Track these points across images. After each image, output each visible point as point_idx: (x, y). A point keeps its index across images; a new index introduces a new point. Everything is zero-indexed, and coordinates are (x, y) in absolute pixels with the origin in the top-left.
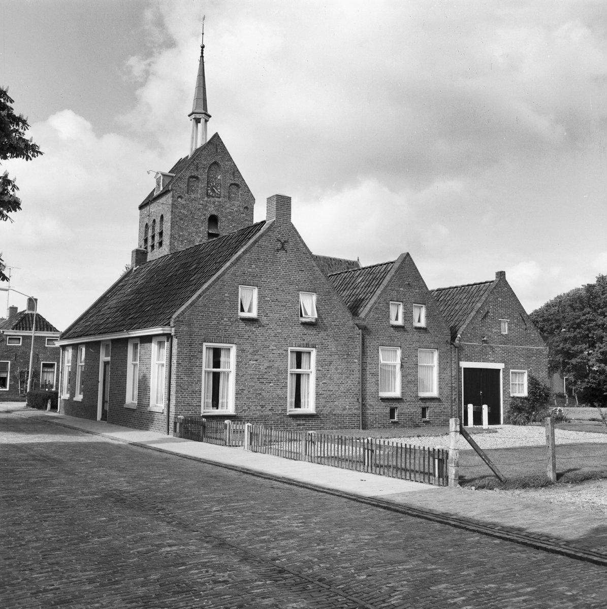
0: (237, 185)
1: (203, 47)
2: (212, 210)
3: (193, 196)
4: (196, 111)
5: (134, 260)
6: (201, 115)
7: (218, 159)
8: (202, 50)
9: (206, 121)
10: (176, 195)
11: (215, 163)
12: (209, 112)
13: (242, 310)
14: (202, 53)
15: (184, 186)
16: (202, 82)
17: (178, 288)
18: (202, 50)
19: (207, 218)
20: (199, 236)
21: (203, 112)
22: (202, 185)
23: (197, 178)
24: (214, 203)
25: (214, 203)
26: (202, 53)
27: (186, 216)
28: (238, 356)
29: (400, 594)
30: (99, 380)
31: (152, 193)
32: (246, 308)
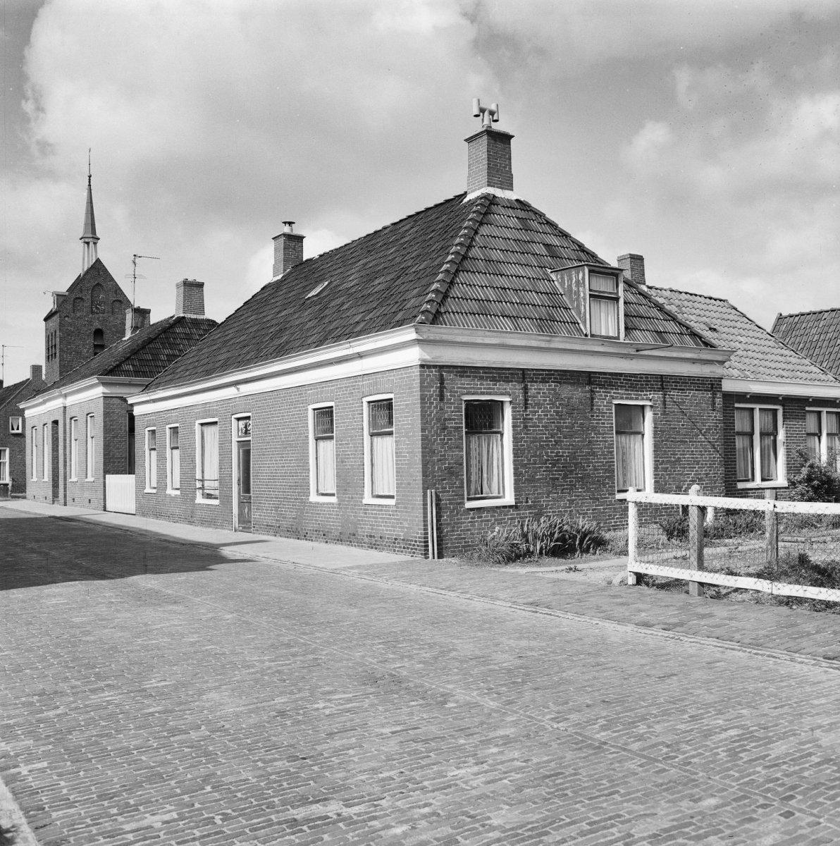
0: (120, 301)
1: (90, 177)
2: (97, 325)
3: (78, 314)
4: (86, 236)
5: (282, 257)
6: (91, 237)
7: (100, 280)
8: (90, 179)
9: (95, 243)
10: (63, 315)
11: (98, 284)
12: (98, 235)
13: (13, 429)
14: (90, 182)
15: (70, 307)
16: (90, 208)
17: (337, 328)
18: (90, 179)
19: (93, 333)
20: (86, 348)
21: (91, 236)
22: (88, 304)
23: (81, 299)
24: (98, 318)
25: (98, 318)
26: (90, 182)
27: (73, 332)
28: (10, 454)
29: (61, 595)
30: (472, 479)
31: (52, 310)
32: (15, 427)
